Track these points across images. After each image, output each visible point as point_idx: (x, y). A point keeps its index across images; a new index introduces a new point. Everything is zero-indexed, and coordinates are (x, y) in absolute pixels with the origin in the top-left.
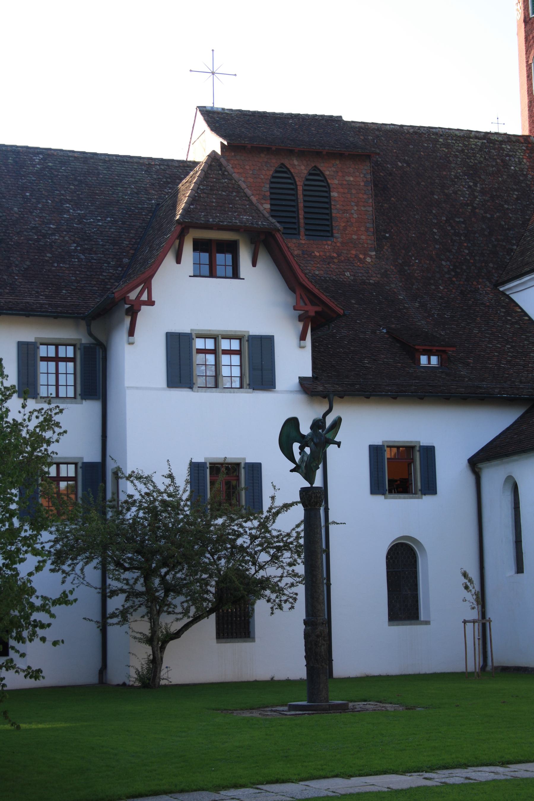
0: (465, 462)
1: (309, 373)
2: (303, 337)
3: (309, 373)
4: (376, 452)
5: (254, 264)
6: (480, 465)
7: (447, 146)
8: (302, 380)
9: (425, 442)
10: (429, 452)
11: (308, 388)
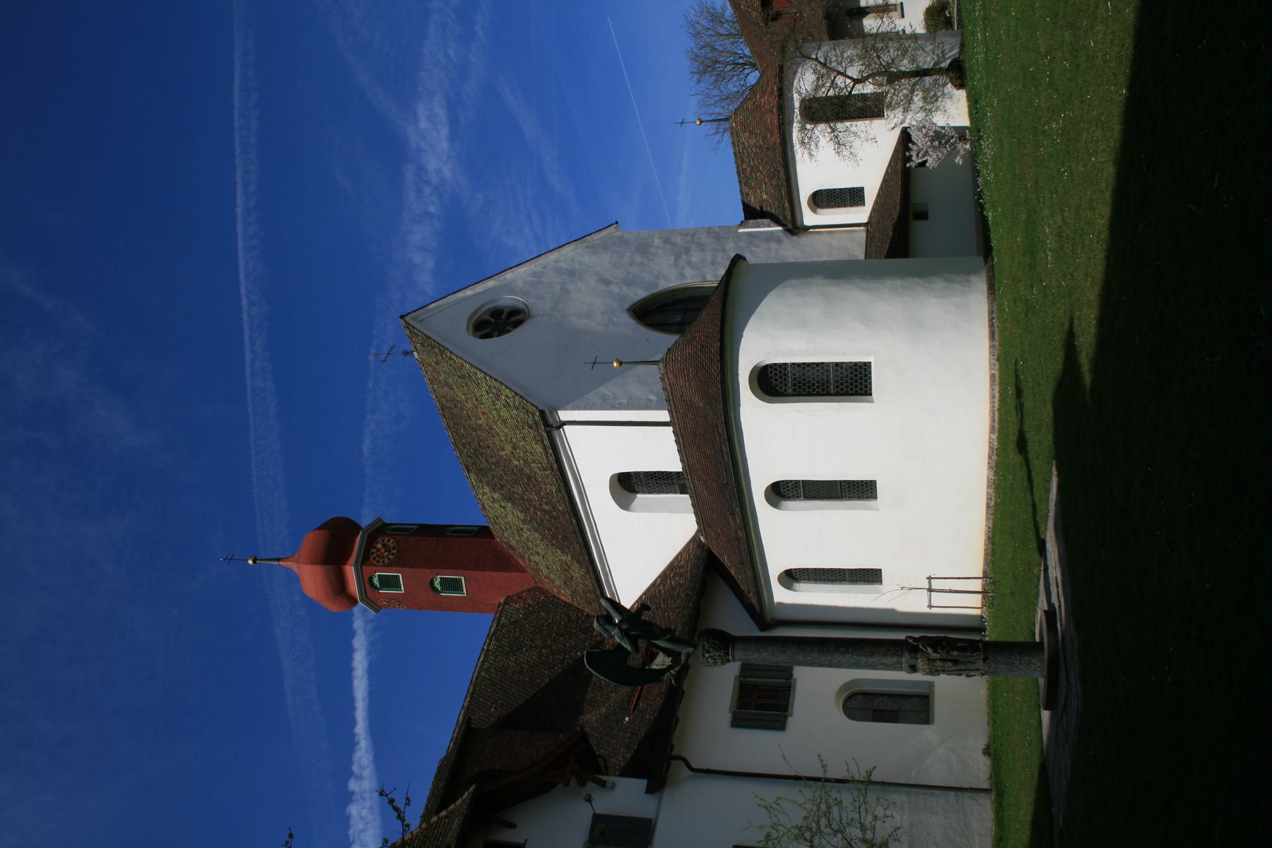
1: (642, 783)
2: (603, 784)
3: (642, 783)
4: (739, 721)
5: (513, 826)
6: (768, 618)
7: (487, 670)
8: (650, 790)
11: (656, 785)
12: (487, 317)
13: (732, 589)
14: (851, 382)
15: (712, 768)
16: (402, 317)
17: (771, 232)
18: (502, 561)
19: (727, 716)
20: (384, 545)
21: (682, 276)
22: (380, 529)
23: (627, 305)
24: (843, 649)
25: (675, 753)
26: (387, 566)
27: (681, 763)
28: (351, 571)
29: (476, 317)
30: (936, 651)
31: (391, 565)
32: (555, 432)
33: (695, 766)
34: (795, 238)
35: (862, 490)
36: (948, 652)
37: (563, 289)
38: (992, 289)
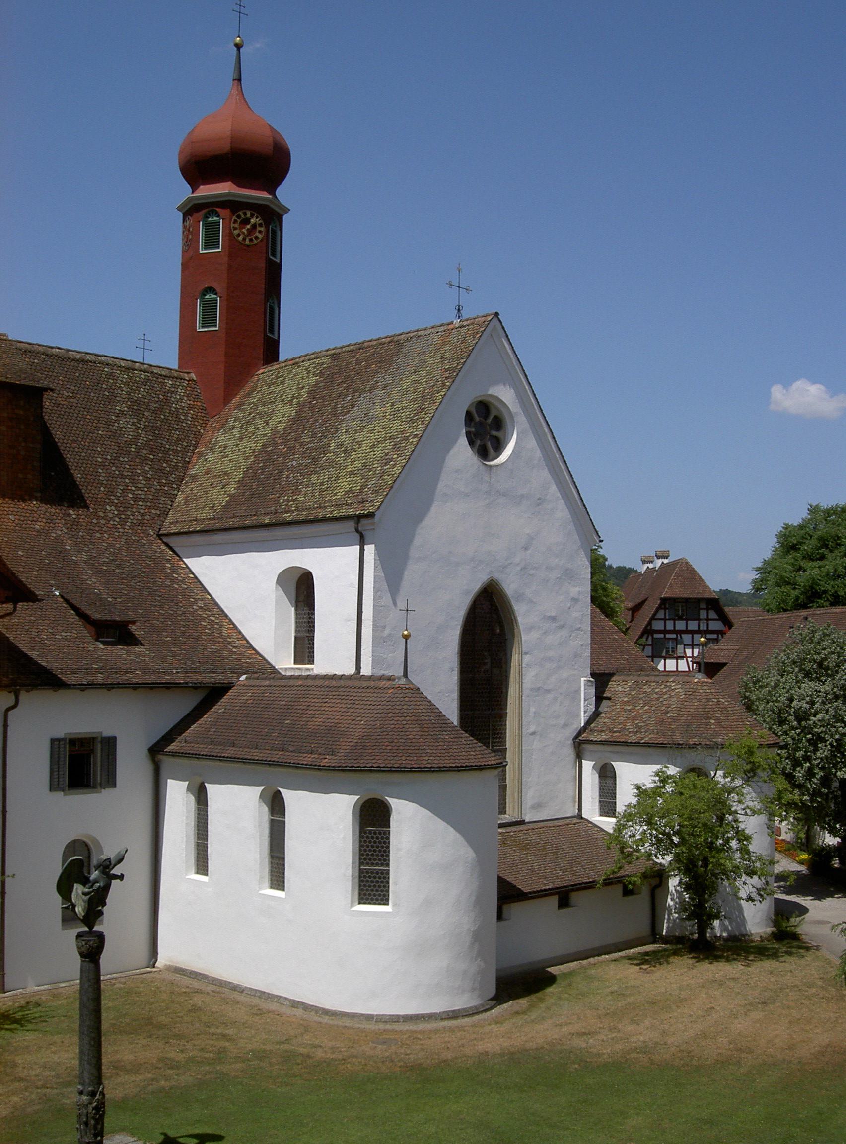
0: (145, 752)
9: (107, 733)
10: (110, 743)
12: (493, 413)
13: (196, 708)
14: (372, 884)
15: (9, 729)
16: (497, 314)
17: (578, 716)
18: (235, 379)
19: (60, 734)
20: (254, 227)
21: (531, 628)
22: (272, 216)
23: (498, 576)
24: (92, 1043)
25: (23, 696)
26: (231, 234)
27: (12, 702)
28: (223, 189)
29: (490, 400)
30: (94, 1109)
31: (230, 236)
32: (351, 525)
33: (10, 713)
34: (570, 742)
35: (278, 879)
36: (93, 1118)
37: (522, 496)
38: (454, 1015)
